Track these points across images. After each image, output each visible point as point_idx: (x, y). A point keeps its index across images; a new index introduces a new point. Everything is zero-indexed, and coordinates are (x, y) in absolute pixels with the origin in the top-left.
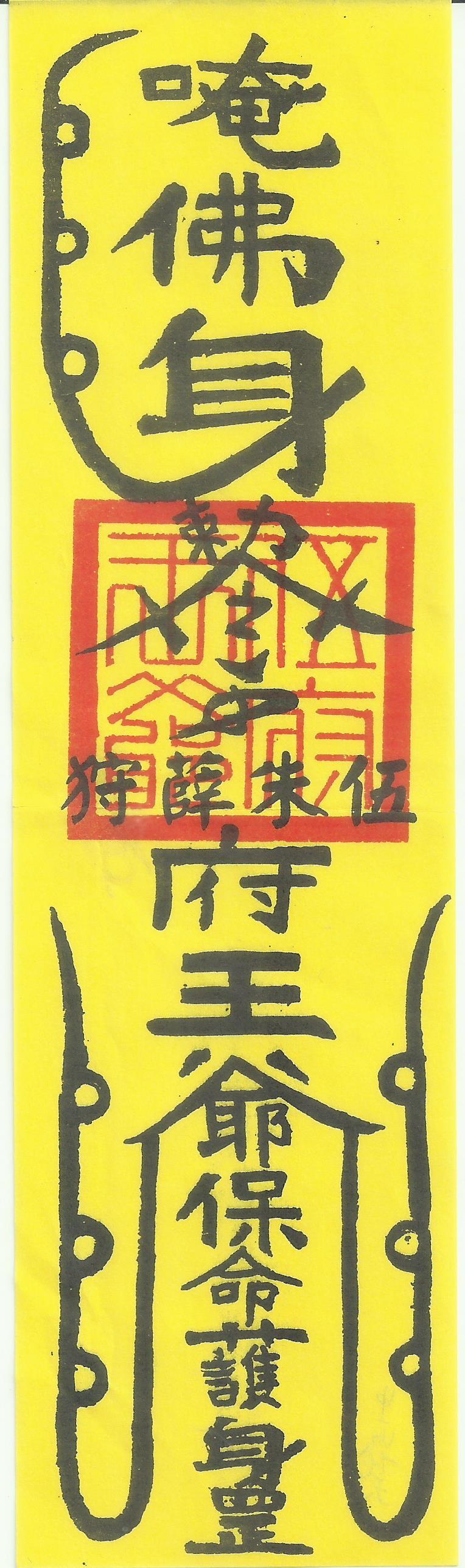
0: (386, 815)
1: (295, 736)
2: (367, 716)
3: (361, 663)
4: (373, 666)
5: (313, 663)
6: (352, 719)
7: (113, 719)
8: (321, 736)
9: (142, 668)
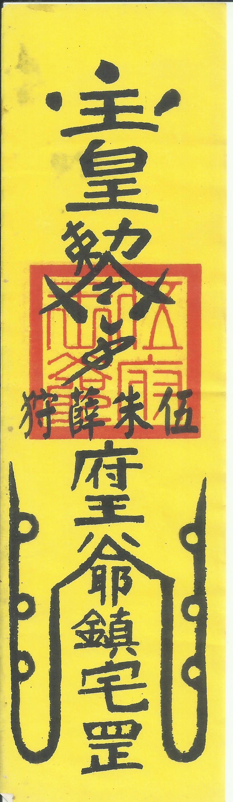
0: (186, 424)
1: (143, 384)
2: (179, 373)
3: (175, 346)
4: (181, 348)
5: (151, 347)
6: (171, 375)
7: (51, 377)
8: (156, 384)
9: (66, 351)
